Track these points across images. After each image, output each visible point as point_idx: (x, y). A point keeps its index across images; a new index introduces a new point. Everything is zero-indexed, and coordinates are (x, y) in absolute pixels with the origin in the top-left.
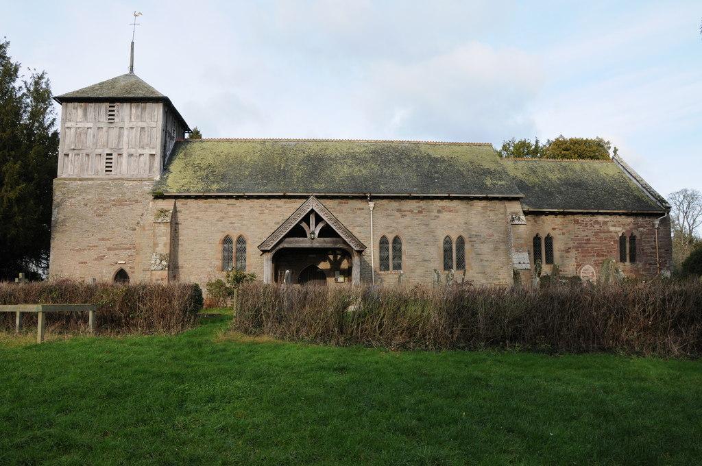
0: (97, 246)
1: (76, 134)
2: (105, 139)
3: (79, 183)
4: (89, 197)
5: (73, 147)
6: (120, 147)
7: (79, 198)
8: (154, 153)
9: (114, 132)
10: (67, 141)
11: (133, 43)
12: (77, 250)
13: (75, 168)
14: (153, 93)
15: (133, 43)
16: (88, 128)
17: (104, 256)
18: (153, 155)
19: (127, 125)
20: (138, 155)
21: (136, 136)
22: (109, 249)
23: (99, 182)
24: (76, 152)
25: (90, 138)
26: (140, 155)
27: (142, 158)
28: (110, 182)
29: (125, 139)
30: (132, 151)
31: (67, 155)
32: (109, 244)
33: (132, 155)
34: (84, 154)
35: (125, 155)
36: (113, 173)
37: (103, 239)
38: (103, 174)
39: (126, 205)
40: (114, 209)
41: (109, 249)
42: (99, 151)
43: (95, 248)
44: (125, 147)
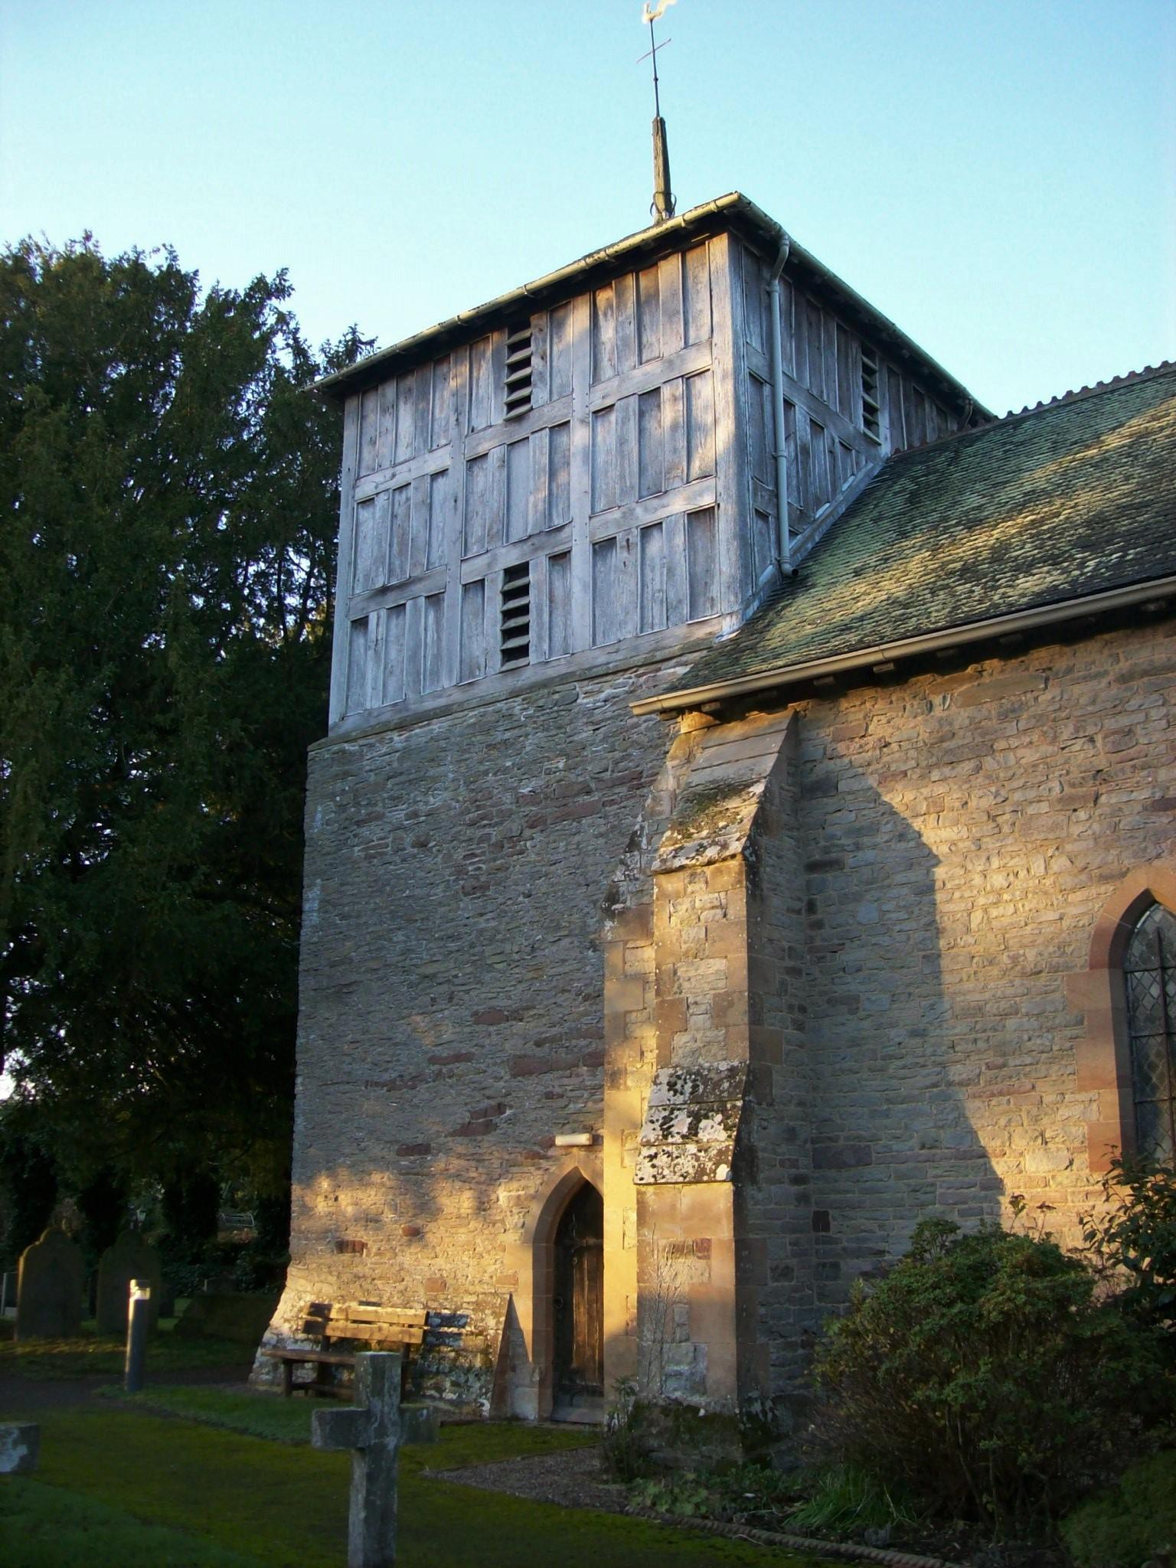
0: (467, 1058)
1: (394, 516)
2: (495, 501)
3: (398, 739)
4: (434, 801)
5: (380, 583)
6: (558, 522)
7: (399, 814)
8: (707, 501)
9: (534, 454)
10: (365, 562)
11: (660, 126)
12: (391, 1086)
13: (388, 672)
14: (746, 321)
15: (660, 126)
16: (436, 476)
17: (500, 1108)
18: (701, 516)
19: (580, 404)
20: (635, 536)
21: (622, 442)
22: (522, 1068)
23: (472, 717)
24: (391, 600)
25: (446, 520)
26: (646, 531)
27: (656, 545)
28: (517, 706)
29: (577, 478)
30: (609, 524)
31: (361, 624)
32: (515, 1038)
33: (611, 542)
34: (422, 600)
35: (454, 595)
36: (533, 658)
37: (494, 1017)
38: (492, 679)
39: (590, 810)
40: (536, 840)
41: (522, 1068)
42: (471, 571)
43: (462, 1066)
44: (579, 508)
